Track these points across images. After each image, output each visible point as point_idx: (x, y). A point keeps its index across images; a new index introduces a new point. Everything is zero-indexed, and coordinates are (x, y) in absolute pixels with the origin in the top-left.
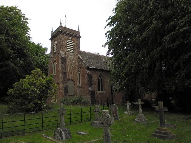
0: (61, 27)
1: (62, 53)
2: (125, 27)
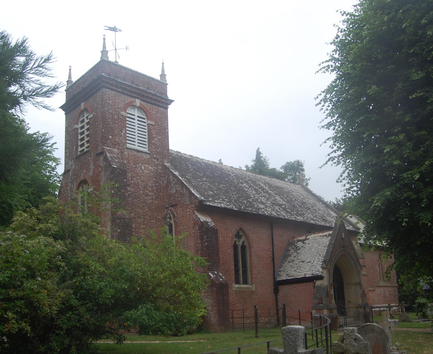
0: (104, 63)
1: (111, 153)
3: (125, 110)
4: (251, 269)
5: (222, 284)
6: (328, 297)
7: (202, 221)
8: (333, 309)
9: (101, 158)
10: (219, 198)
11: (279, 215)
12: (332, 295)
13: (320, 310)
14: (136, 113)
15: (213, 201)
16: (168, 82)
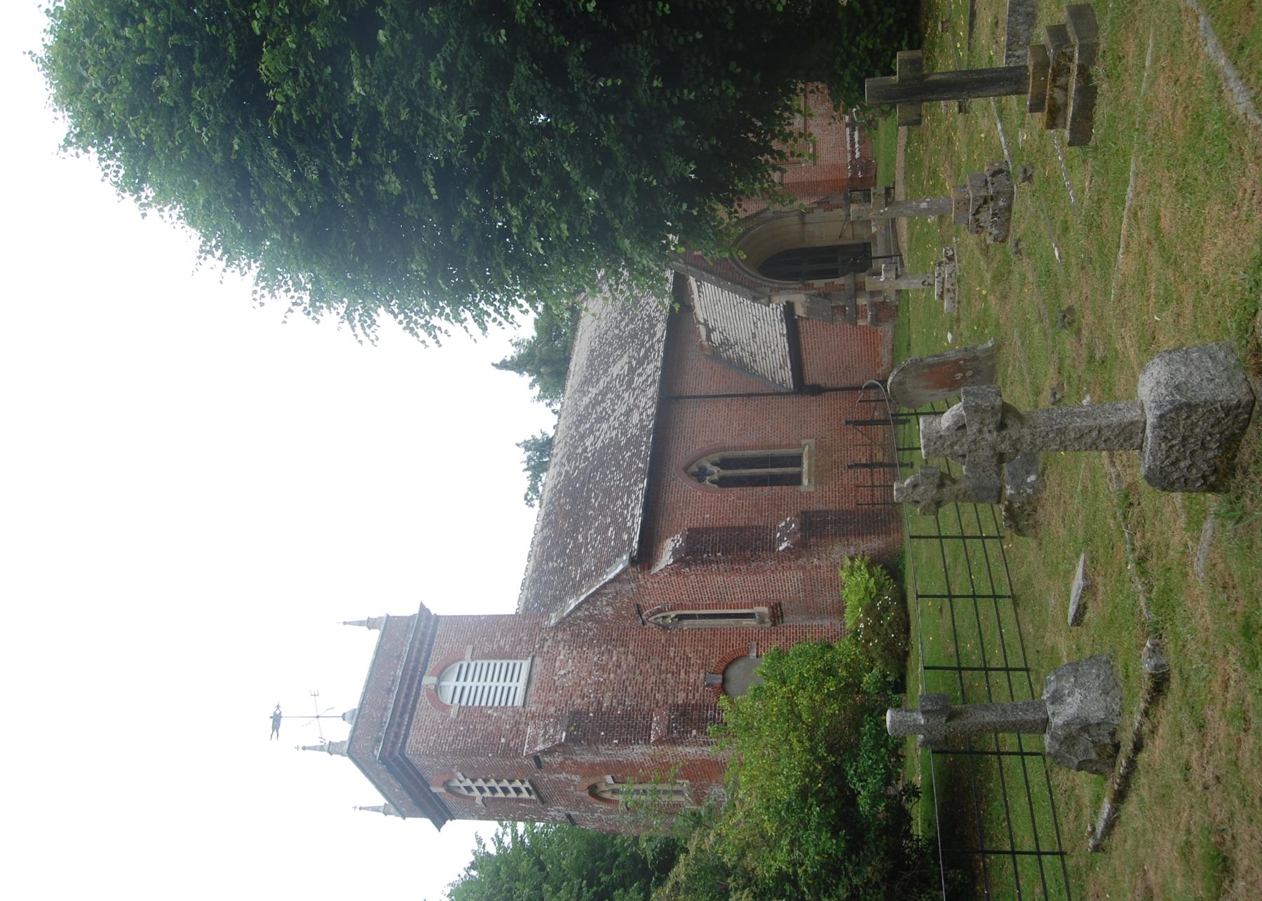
0: (354, 750)
1: (536, 739)
3: (446, 708)
4: (769, 447)
8: (856, 284)
10: (622, 514)
11: (654, 381)
13: (857, 311)
14: (450, 684)
15: (629, 530)
16: (383, 615)
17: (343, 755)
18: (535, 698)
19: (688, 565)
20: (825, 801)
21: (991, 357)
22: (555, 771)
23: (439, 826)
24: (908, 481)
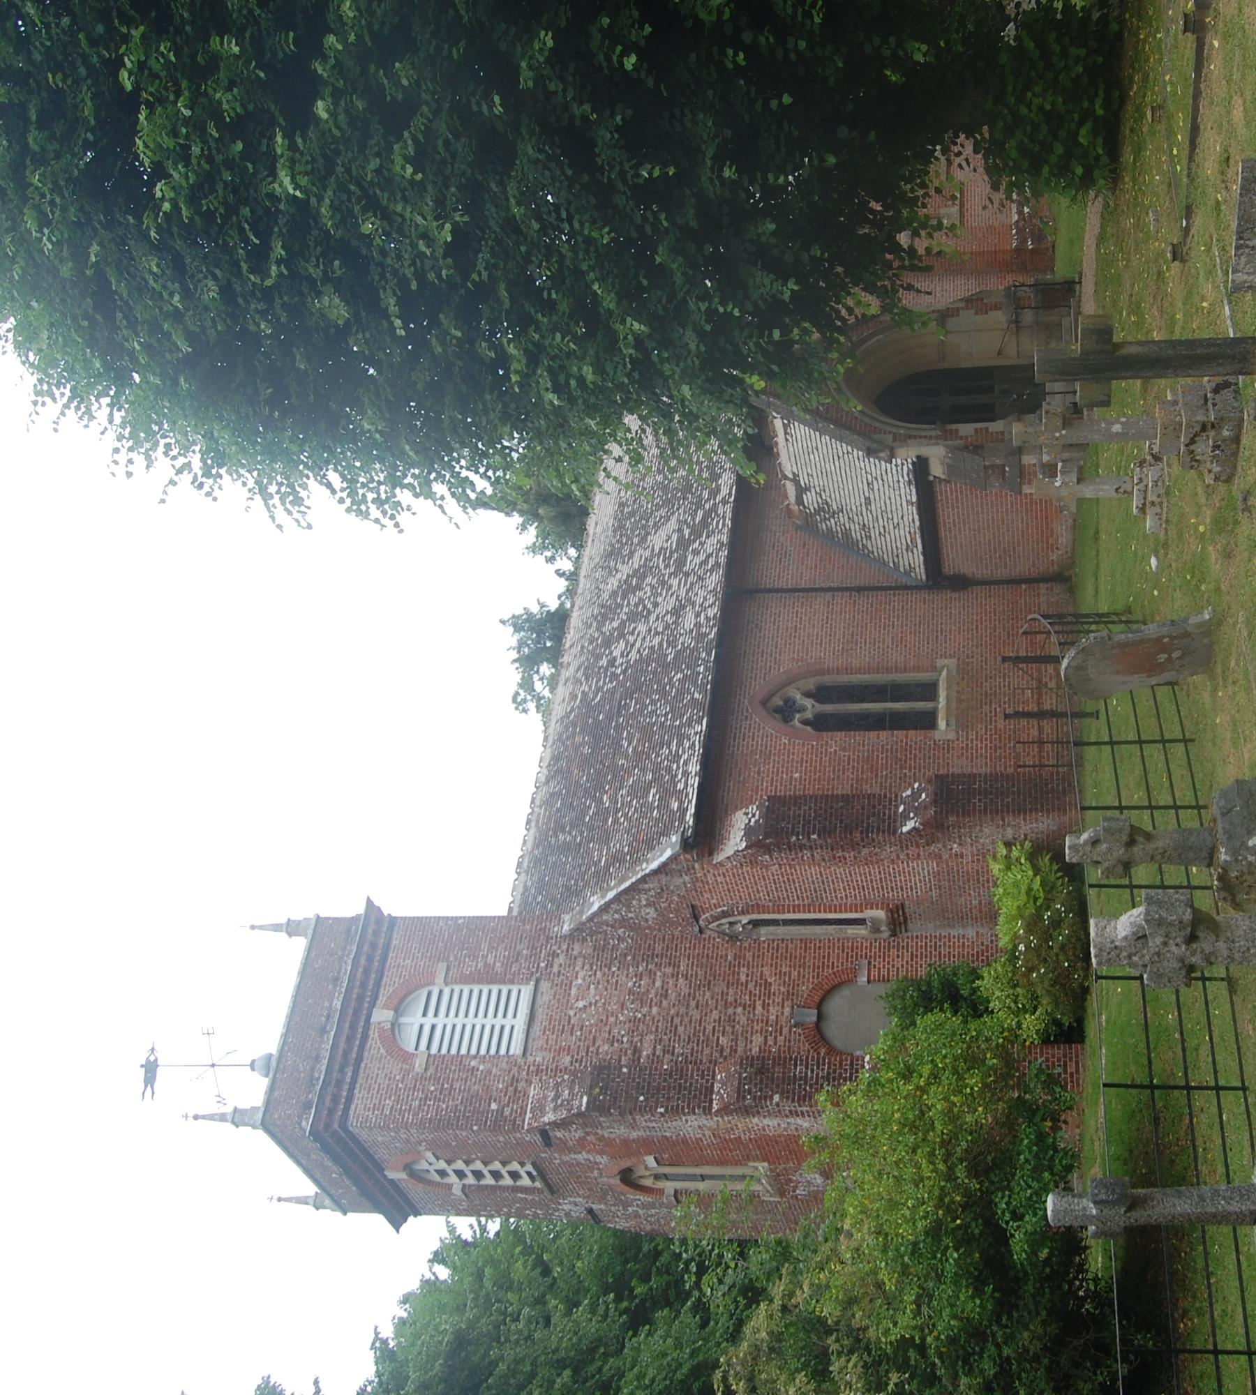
0: (272, 1120)
1: (544, 1104)
2: (267, 313)
3: (407, 1057)
4: (888, 670)
5: (936, 795)
6: (982, 447)
7: (744, 844)
9: (559, 1134)
10: (669, 770)
11: (717, 564)
12: (976, 430)
14: (413, 1020)
15: (681, 796)
16: (311, 915)
17: (254, 1127)
18: (541, 1042)
19: (769, 851)
20: (964, 1240)
21: (1208, 633)
22: (571, 1150)
23: (397, 1224)
24: (1085, 836)
